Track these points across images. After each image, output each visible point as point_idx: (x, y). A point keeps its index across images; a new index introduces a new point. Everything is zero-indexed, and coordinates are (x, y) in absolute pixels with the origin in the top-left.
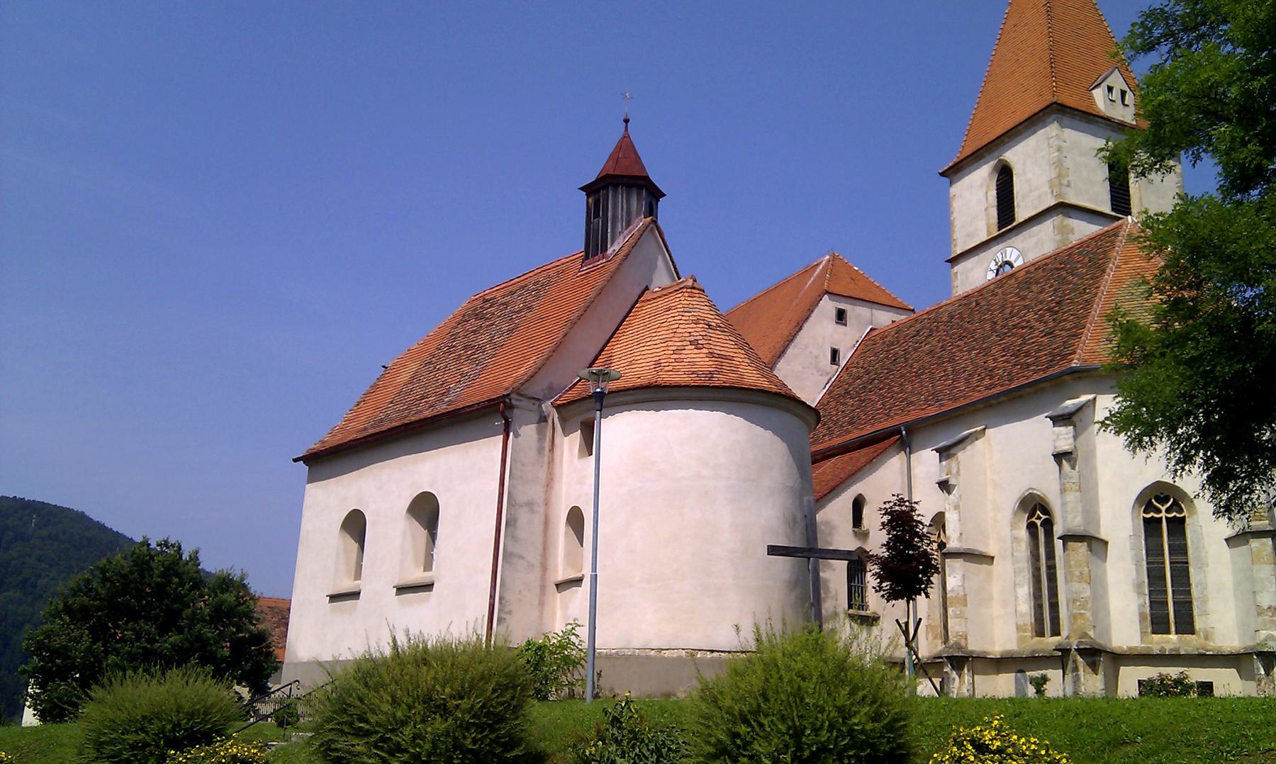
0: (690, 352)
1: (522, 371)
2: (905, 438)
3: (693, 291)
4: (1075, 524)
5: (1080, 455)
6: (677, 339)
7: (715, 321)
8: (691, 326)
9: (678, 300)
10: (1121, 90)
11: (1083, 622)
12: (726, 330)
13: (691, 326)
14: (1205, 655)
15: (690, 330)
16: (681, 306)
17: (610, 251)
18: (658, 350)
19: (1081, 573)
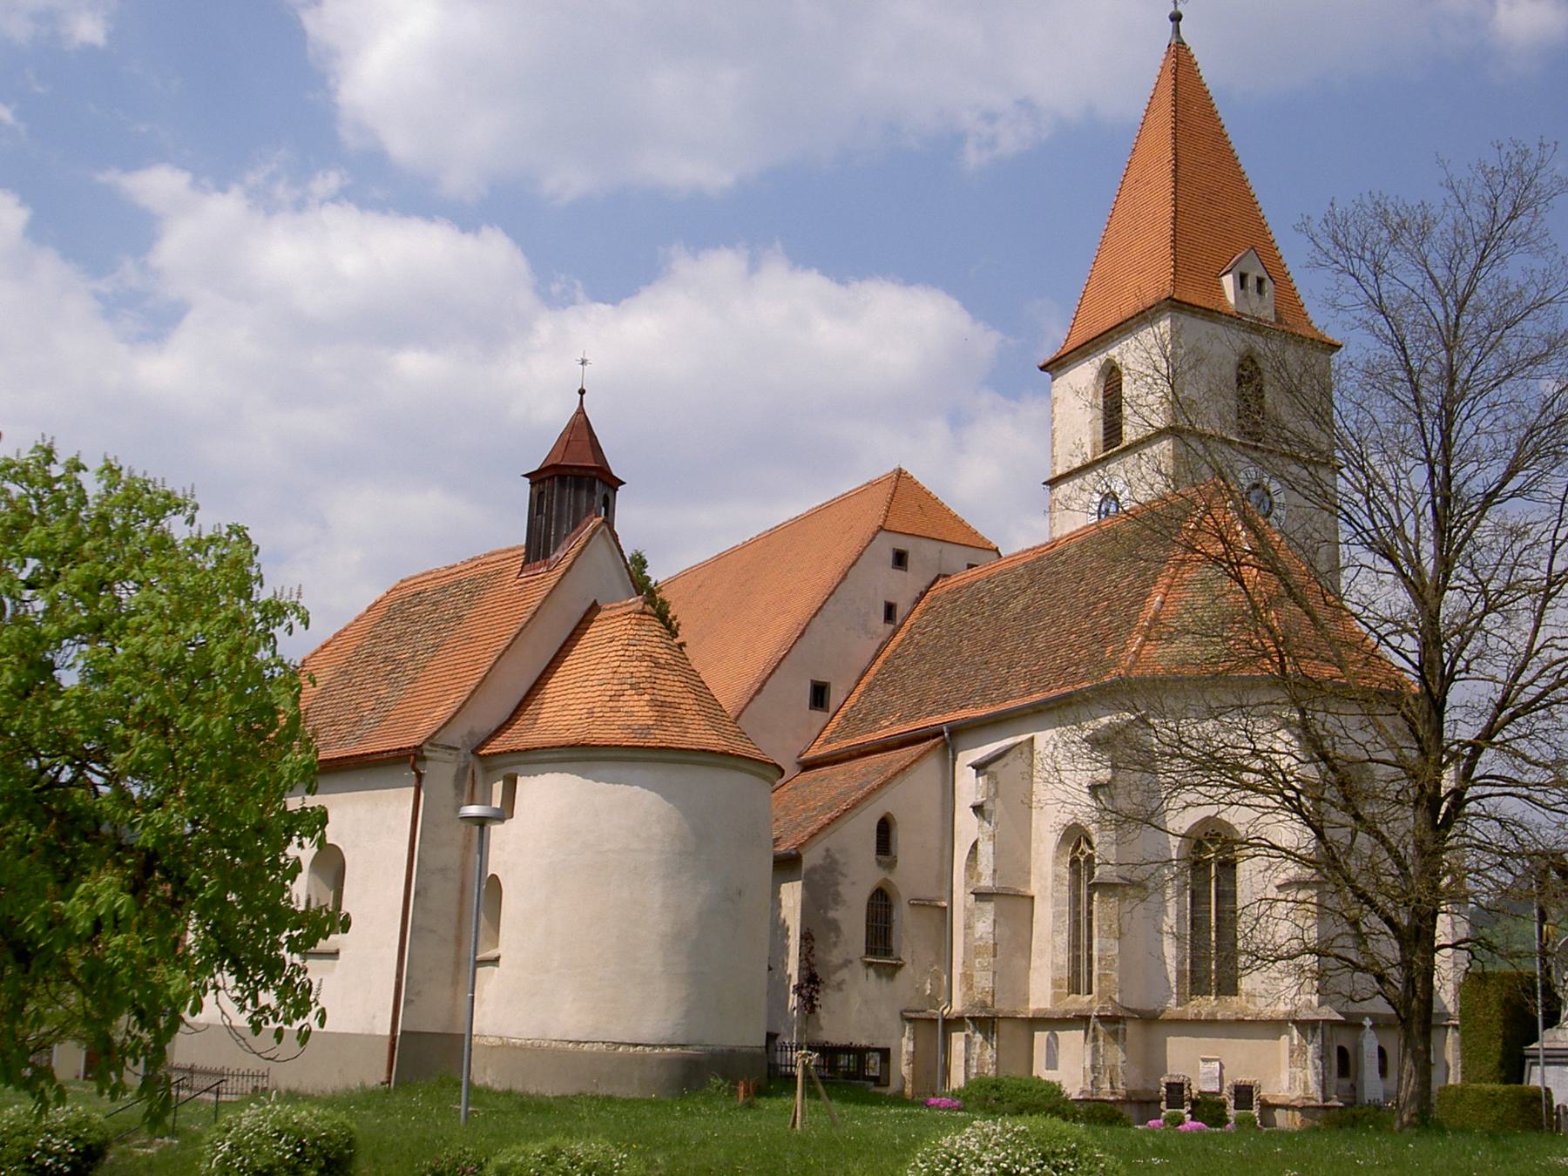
0: (629, 698)
1: (439, 712)
2: (948, 741)
3: (642, 617)
6: (616, 682)
7: (665, 656)
8: (635, 664)
9: (624, 628)
10: (1258, 278)
12: (676, 668)
13: (635, 664)
14: (1243, 1020)
15: (632, 670)
16: (625, 637)
17: (553, 557)
18: (593, 695)
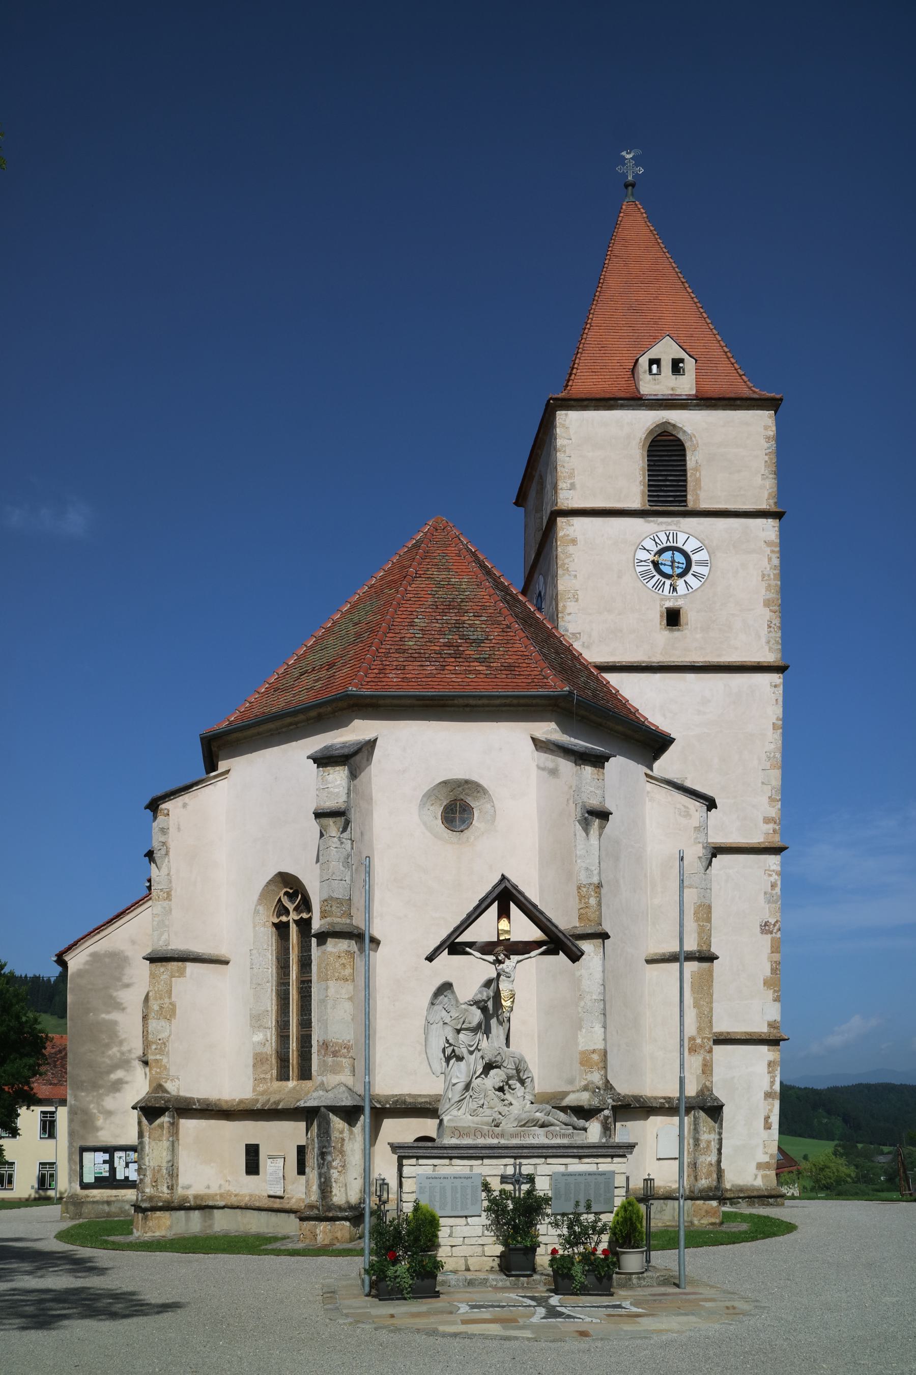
4: (161, 943)
5: (353, 816)
11: (158, 1070)
19: (161, 1008)
